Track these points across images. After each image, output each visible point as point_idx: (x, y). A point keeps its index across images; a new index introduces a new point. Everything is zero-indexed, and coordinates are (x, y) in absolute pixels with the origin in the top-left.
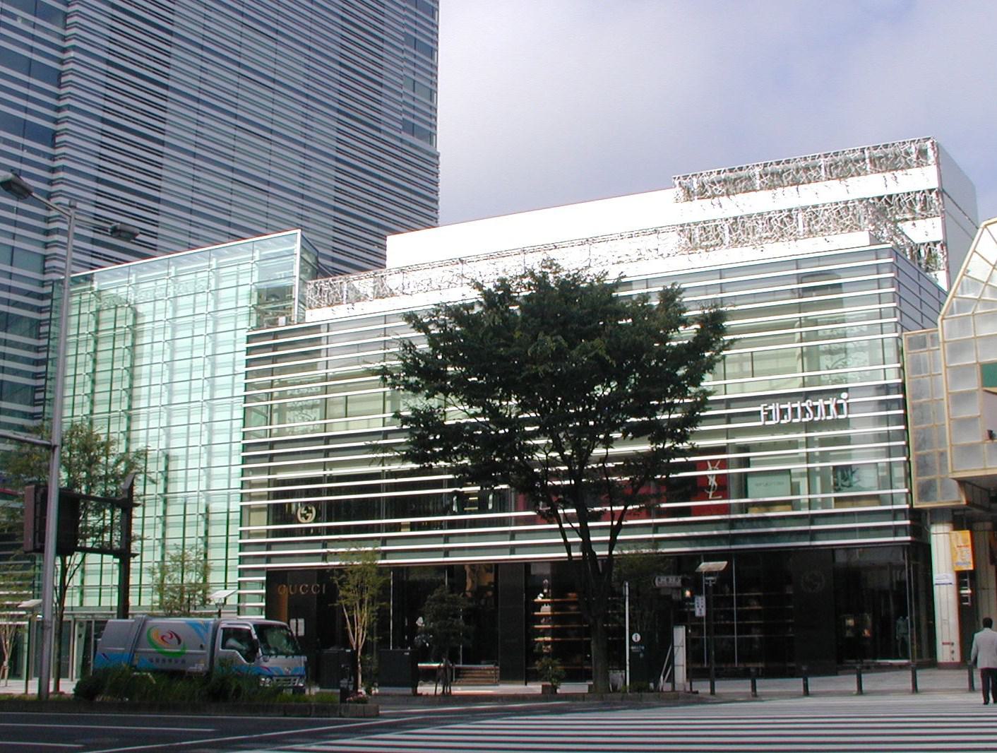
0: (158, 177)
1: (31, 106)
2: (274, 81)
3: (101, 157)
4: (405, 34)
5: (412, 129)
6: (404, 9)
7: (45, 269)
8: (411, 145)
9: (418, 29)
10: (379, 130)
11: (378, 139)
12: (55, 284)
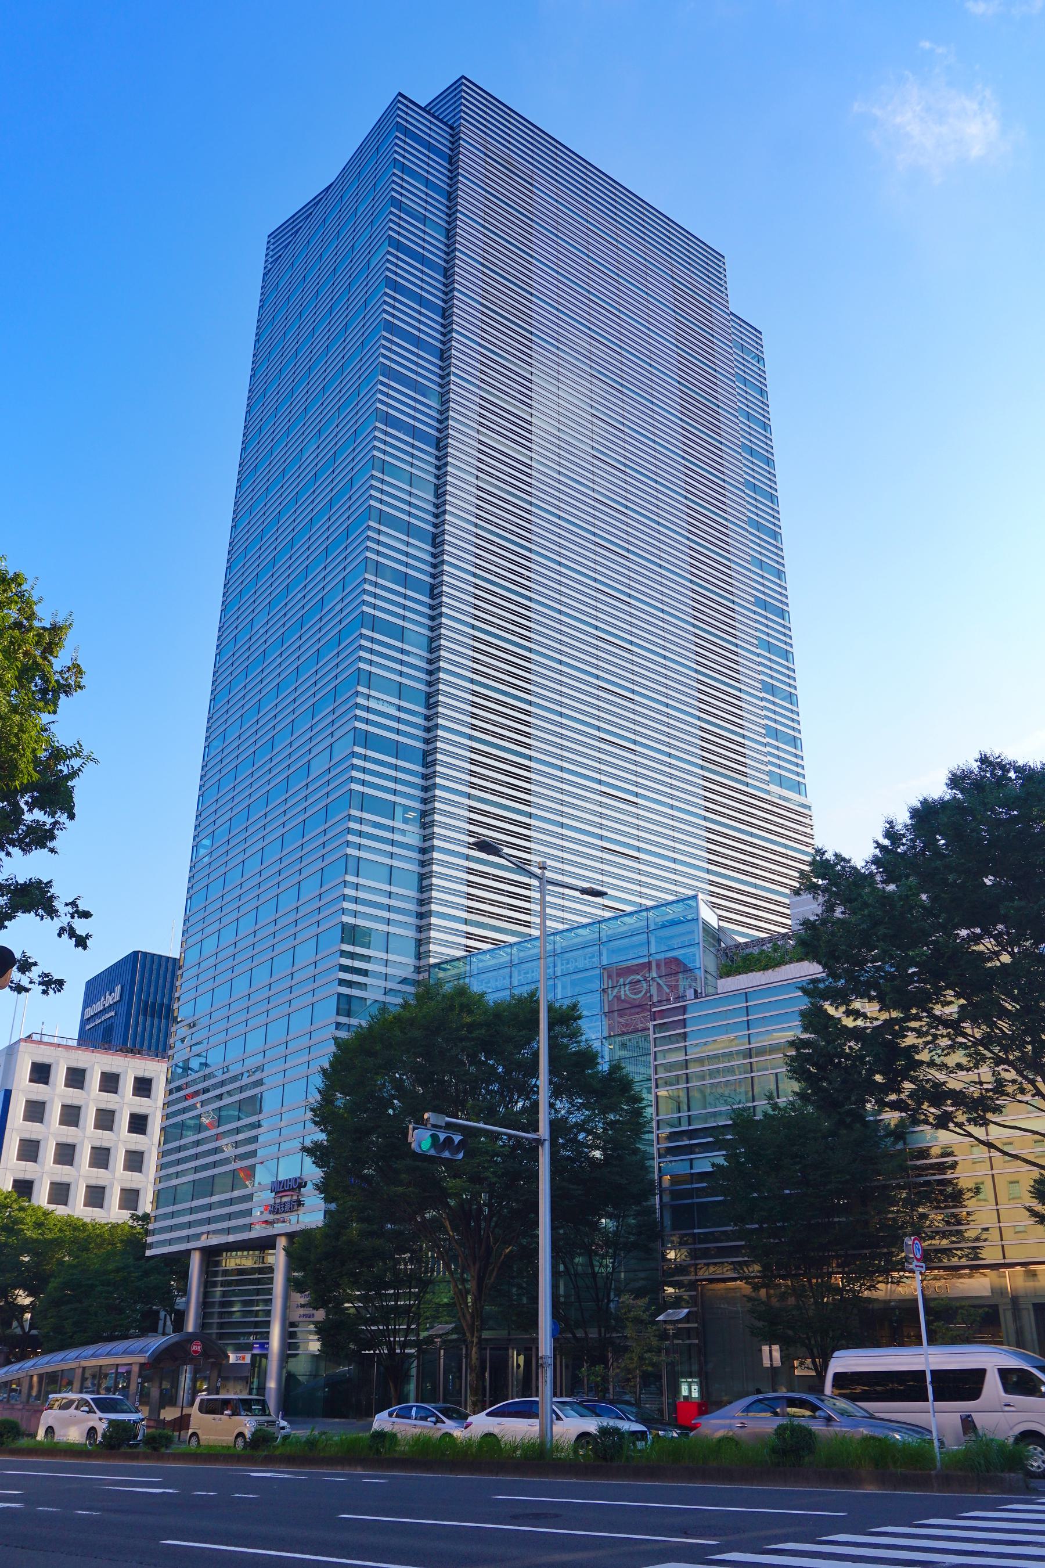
0: (528, 792)
1: (419, 406)
2: (631, 643)
3: (470, 884)
4: (761, 681)
5: (781, 781)
6: (765, 745)
7: (420, 954)
8: (781, 797)
9: (770, 632)
10: (747, 785)
11: (745, 793)
12: (432, 970)
